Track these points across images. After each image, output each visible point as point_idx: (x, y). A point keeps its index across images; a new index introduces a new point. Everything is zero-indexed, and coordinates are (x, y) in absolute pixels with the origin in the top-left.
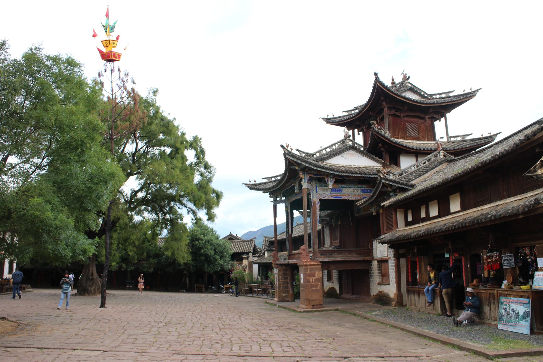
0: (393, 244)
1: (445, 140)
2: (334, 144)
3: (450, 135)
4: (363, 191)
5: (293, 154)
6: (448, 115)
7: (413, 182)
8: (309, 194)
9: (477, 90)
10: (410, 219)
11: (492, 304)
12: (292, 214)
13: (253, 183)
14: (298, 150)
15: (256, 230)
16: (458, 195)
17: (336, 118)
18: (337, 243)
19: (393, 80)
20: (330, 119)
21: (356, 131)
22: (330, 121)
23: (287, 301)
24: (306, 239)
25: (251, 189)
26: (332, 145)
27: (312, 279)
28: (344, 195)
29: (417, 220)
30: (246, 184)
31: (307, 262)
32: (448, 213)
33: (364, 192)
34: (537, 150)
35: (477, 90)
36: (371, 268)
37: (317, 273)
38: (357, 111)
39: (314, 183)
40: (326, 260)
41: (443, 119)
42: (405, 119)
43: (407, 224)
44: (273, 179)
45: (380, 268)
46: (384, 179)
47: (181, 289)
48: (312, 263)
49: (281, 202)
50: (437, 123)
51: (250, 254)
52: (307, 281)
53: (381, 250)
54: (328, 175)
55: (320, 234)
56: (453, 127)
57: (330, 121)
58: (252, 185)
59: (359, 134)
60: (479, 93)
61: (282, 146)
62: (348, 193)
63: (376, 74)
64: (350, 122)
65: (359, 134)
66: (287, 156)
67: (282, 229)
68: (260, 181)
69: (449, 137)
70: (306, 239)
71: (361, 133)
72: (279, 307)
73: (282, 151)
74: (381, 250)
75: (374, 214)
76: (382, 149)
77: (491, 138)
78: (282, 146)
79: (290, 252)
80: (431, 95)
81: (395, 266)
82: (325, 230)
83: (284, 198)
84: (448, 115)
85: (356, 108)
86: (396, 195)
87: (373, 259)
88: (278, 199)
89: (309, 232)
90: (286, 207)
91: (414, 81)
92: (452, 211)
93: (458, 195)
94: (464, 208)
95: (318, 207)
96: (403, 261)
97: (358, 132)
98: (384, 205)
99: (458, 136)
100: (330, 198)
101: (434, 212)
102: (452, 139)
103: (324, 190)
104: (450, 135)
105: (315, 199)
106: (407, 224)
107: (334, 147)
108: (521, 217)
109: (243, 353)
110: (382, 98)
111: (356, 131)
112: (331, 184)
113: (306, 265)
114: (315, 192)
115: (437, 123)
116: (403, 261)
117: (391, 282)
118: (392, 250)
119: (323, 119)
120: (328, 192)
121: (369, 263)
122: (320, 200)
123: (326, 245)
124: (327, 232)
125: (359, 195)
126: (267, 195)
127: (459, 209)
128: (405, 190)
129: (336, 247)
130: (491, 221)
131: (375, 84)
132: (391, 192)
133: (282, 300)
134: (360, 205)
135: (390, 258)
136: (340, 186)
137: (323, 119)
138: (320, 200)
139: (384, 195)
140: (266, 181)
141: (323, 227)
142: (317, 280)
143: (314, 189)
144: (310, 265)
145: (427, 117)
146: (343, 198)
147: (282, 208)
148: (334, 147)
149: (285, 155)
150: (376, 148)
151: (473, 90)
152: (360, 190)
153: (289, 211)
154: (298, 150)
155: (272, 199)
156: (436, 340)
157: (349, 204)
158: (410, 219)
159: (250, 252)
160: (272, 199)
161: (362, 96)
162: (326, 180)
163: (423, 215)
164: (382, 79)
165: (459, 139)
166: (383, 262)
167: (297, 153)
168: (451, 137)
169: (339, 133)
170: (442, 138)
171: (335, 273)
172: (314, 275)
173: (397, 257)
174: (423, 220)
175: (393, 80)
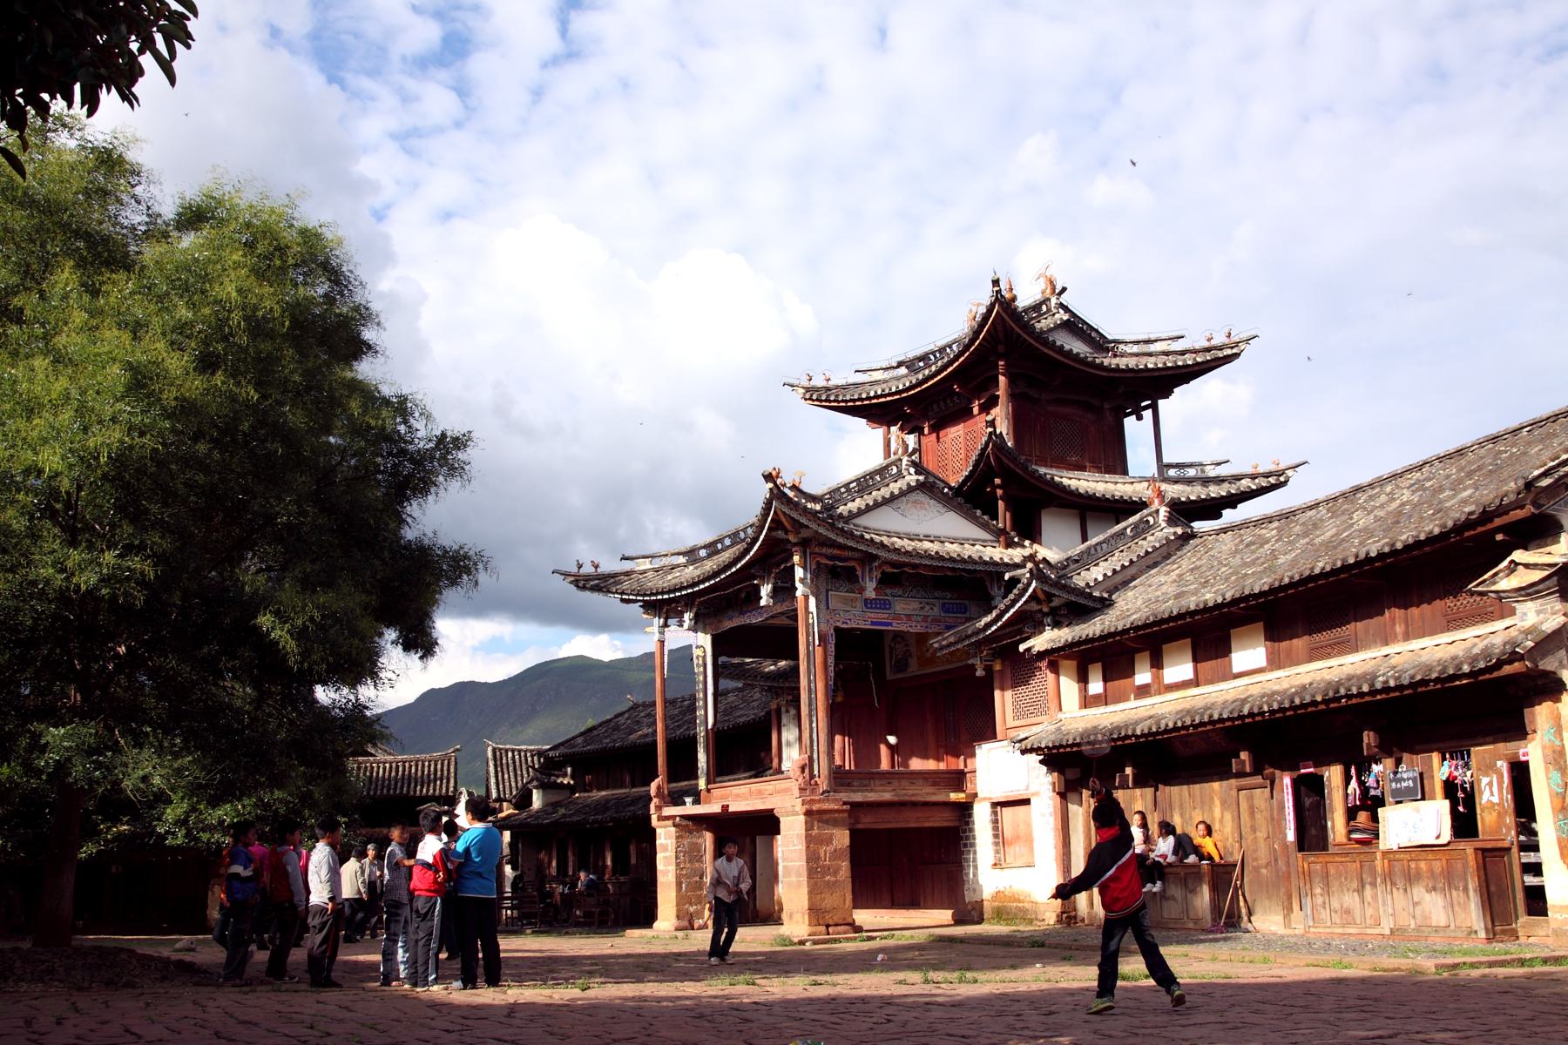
3: (1166, 460)
11: (1368, 887)
13: (588, 569)
28: (897, 617)
30: (566, 574)
33: (947, 611)
34: (1499, 537)
36: (967, 823)
42: (1050, 408)
43: (1087, 701)
48: (826, 806)
50: (1130, 422)
54: (868, 559)
58: (588, 578)
60: (1248, 352)
62: (906, 614)
75: (980, 673)
92: (1236, 670)
98: (1029, 650)
99: (1191, 465)
102: (1172, 472)
103: (845, 601)
104: (1166, 460)
106: (1087, 701)
110: (1001, 348)
115: (1130, 422)
121: (965, 809)
122: (837, 629)
125: (936, 621)
127: (1263, 663)
130: (1386, 689)
134: (942, 648)
136: (888, 591)
138: (837, 629)
145: (1106, 406)
152: (938, 603)
162: (859, 573)
168: (1170, 466)
172: (829, 841)
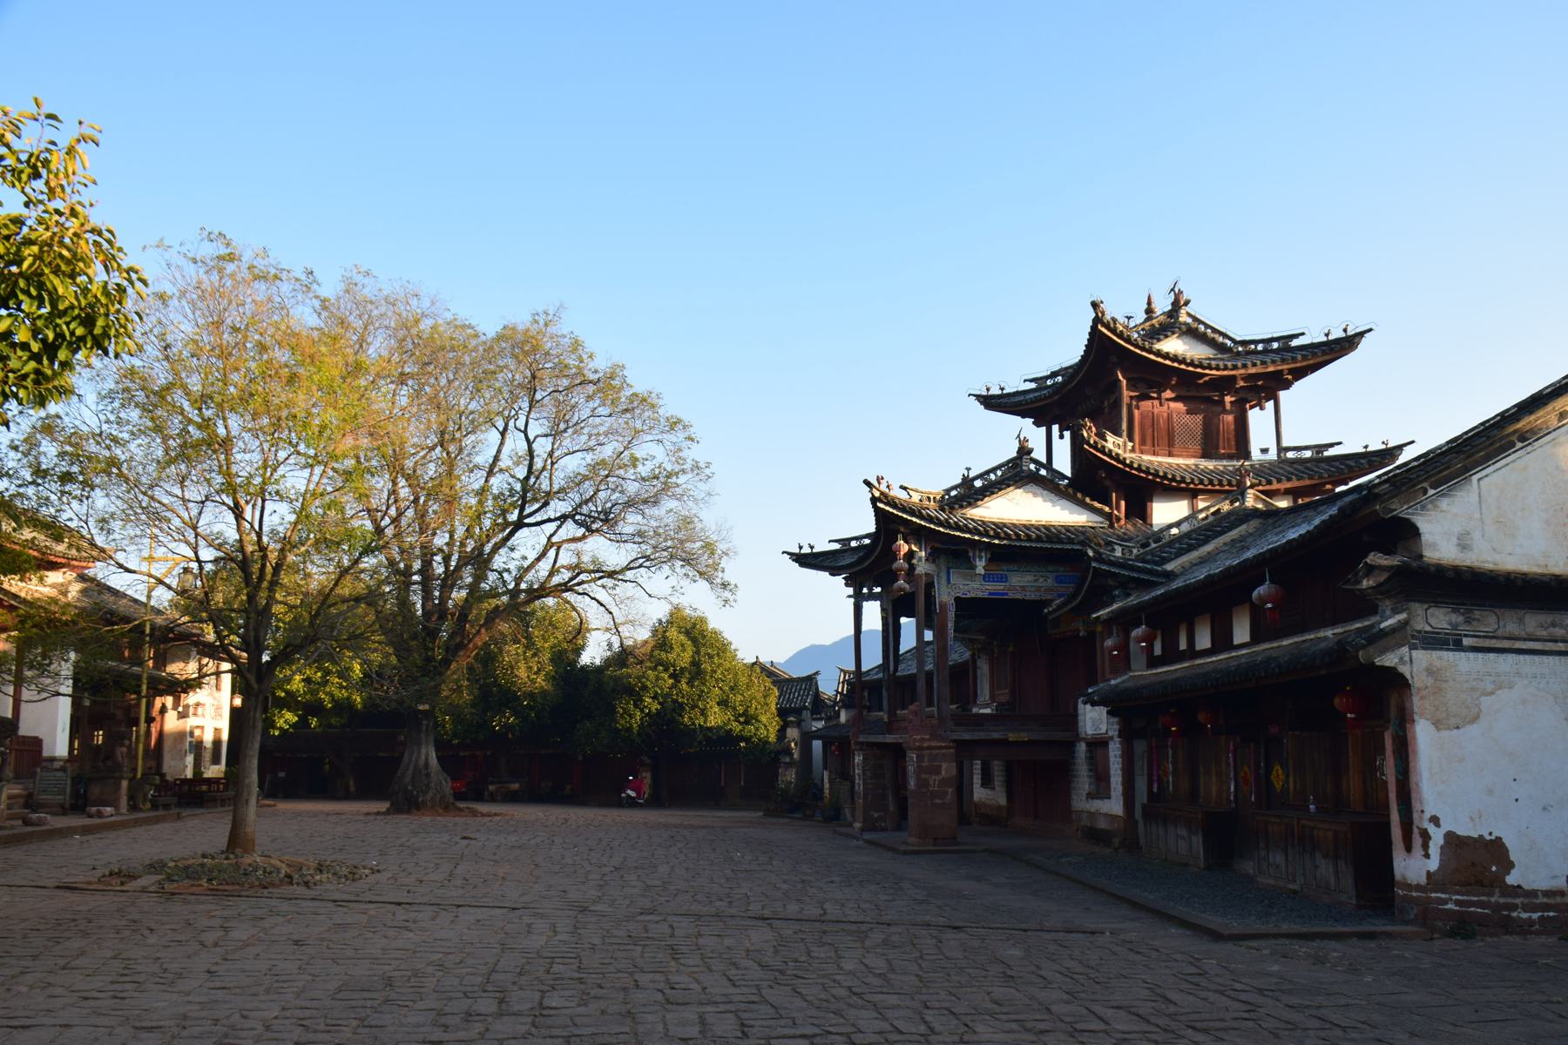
0: (1117, 705)
1: (1272, 455)
2: (993, 470)
4: (1058, 580)
5: (893, 499)
6: (1282, 394)
7: (1169, 567)
8: (930, 586)
9: (1362, 334)
10: (1158, 651)
12: (897, 627)
13: (806, 550)
14: (903, 488)
15: (828, 642)
16: (1208, 617)
17: (1009, 395)
18: (1004, 695)
19: (1149, 303)
20: (993, 397)
21: (1055, 428)
22: (991, 402)
23: (883, 830)
24: (921, 684)
25: (802, 564)
26: (988, 472)
27: (934, 780)
28: (1014, 588)
29: (1171, 655)
31: (923, 740)
32: (1230, 646)
35: (1362, 334)
37: (944, 766)
38: (1060, 379)
39: (942, 561)
40: (967, 736)
41: (1270, 405)
44: (854, 544)
45: (1091, 759)
46: (1095, 559)
47: (1451, 574)
49: (872, 597)
51: (806, 714)
52: (923, 784)
53: (1094, 719)
55: (961, 678)
56: (1310, 418)
57: (991, 402)
59: (1061, 437)
61: (867, 483)
62: (1022, 583)
63: (1095, 305)
64: (1046, 403)
65: (1061, 437)
66: (880, 505)
67: (873, 658)
68: (822, 546)
69: (1281, 450)
70: (921, 684)
71: (1067, 434)
72: (869, 842)
73: (866, 494)
74: (1094, 719)
76: (1108, 483)
77: (1389, 453)
78: (867, 483)
79: (892, 714)
80: (1244, 343)
81: (1123, 756)
82: (979, 663)
83: (878, 590)
84: (1282, 394)
85: (1054, 375)
86: (1129, 595)
87: (1077, 738)
88: (865, 590)
89: (929, 667)
90: (883, 610)
91: (1206, 308)
92: (1236, 642)
93: (1208, 617)
94: (1256, 638)
95: (951, 615)
96: (1140, 747)
97: (1061, 431)
100: (980, 595)
101: (1204, 641)
102: (1290, 455)
104: (1285, 444)
105: (945, 595)
106: (1153, 662)
107: (992, 477)
108: (1323, 672)
109: (767, 913)
111: (1055, 428)
112: (981, 566)
113: (921, 748)
114: (944, 581)
116: (1140, 747)
117: (1113, 794)
118: (1115, 720)
119: (978, 397)
120: (974, 583)
121: (1070, 746)
122: (957, 599)
123: (980, 700)
124: (984, 667)
125: (1049, 590)
126: (839, 580)
128: (1152, 585)
129: (1000, 705)
131: (1094, 333)
132: (1116, 588)
133: (870, 826)
135: (1112, 738)
137: (978, 397)
138: (957, 599)
139: (1100, 595)
140: (837, 546)
141: (973, 656)
142: (943, 782)
143: (943, 575)
144: (929, 748)
146: (1011, 595)
147: (873, 613)
148: (992, 477)
149: (874, 500)
150: (1091, 479)
151: (1350, 333)
153: (890, 620)
154: (903, 488)
155: (850, 591)
156: (1120, 898)
157: (1028, 611)
158: (1158, 651)
159: (805, 708)
160: (850, 591)
161: (1066, 348)
163: (1183, 646)
164: (1112, 311)
165: (1308, 454)
166: (1098, 745)
167: (903, 495)
169: (1006, 435)
170: (1265, 451)
171: (997, 768)
172: (937, 771)
173: (1127, 735)
174: (1182, 656)
175: (1149, 303)
